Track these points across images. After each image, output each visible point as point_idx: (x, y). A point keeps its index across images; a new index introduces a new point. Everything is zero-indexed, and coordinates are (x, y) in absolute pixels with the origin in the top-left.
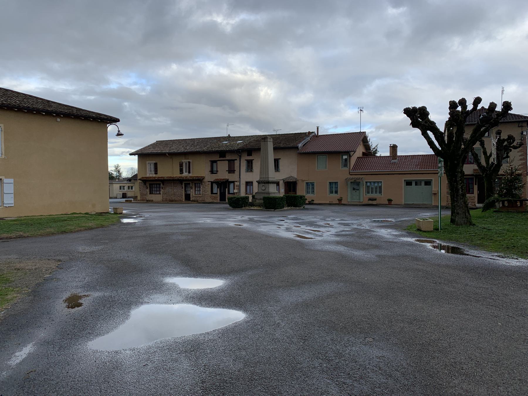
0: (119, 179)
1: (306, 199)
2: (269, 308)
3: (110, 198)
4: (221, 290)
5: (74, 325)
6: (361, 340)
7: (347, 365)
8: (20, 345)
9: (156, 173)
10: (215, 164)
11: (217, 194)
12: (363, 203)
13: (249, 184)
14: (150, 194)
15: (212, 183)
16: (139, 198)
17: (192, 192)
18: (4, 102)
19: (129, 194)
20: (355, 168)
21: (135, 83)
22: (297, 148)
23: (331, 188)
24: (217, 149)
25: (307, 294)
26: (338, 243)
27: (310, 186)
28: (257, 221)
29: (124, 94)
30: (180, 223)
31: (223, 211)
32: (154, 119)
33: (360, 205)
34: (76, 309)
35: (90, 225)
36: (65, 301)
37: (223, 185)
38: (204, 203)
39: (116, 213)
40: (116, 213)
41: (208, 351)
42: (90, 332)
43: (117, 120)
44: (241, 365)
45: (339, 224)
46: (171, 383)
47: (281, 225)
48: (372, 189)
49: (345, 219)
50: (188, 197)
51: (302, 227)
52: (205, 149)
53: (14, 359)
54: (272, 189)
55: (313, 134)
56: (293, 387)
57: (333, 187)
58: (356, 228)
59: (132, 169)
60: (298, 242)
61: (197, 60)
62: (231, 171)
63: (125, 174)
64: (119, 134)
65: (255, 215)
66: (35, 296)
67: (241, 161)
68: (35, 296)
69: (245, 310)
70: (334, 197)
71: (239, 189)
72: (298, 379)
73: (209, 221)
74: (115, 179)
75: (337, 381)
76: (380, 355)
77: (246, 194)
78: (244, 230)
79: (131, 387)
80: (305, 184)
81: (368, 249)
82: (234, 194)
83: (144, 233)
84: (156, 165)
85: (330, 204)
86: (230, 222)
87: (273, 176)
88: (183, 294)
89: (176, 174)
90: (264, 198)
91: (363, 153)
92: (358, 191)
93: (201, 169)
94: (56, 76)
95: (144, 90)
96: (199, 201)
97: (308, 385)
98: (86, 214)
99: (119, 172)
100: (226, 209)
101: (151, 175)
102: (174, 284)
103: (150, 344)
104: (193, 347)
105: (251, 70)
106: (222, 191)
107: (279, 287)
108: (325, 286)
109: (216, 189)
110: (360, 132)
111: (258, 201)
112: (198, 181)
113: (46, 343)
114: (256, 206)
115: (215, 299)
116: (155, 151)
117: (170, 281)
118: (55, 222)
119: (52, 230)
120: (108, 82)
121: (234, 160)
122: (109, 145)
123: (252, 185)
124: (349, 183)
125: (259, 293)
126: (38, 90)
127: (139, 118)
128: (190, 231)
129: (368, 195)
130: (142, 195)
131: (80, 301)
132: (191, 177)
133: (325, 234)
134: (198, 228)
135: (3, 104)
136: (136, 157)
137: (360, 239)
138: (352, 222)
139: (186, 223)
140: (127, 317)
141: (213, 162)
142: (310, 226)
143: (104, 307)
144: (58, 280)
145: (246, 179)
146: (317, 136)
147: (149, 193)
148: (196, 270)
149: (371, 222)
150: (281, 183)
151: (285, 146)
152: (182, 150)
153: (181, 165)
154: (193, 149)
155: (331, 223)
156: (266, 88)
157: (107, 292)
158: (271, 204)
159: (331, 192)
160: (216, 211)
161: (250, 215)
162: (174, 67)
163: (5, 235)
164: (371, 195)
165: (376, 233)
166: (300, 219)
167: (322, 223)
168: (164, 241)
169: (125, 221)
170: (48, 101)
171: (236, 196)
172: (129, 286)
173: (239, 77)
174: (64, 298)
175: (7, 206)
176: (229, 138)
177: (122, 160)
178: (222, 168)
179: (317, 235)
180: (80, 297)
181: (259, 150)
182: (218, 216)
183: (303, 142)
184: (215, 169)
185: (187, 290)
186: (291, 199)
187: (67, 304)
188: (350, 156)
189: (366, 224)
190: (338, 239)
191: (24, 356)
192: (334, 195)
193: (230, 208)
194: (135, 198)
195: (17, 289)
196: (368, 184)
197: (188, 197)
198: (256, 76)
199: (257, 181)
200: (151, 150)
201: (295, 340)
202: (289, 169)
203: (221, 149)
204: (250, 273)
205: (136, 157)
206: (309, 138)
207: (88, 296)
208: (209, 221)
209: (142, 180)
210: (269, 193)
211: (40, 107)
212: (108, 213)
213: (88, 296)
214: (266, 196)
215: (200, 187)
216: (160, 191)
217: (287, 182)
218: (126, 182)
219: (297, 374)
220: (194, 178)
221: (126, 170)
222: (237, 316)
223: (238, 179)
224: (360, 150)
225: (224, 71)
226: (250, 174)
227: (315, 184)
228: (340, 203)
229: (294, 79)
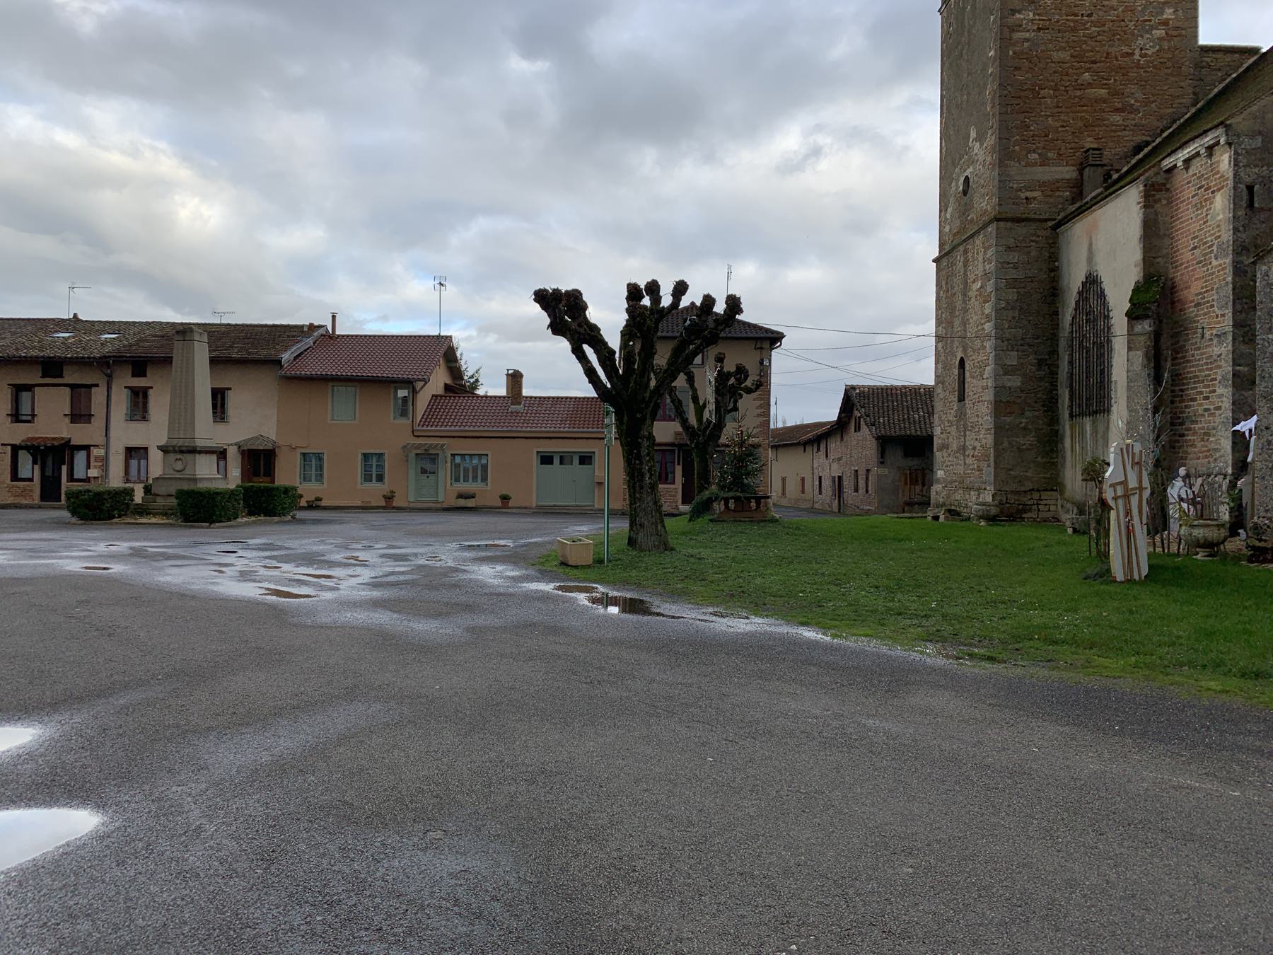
1: (301, 496)
4: (26, 756)
11: (31, 480)
15: (15, 449)
20: (427, 419)
22: (279, 362)
24: (34, 353)
25: (285, 740)
26: (376, 604)
27: (313, 462)
33: (437, 510)
45: (383, 556)
48: (466, 470)
49: (397, 544)
54: (205, 471)
55: (322, 331)
57: (373, 465)
60: (271, 606)
62: (79, 415)
65: (151, 540)
70: (375, 491)
71: (105, 466)
77: (127, 481)
78: (113, 581)
81: (448, 614)
82: (88, 480)
85: (365, 508)
87: (206, 431)
90: (181, 495)
92: (432, 477)
100: (60, 525)
105: (153, 148)
106: (49, 473)
107: (209, 729)
109: (27, 466)
110: (439, 337)
111: (160, 502)
114: (155, 515)
121: (90, 387)
133: (344, 585)
137: (432, 592)
138: (415, 551)
141: (18, 389)
142: (307, 565)
145: (119, 439)
150: (232, 453)
151: (244, 355)
155: (362, 555)
156: (196, 200)
158: (199, 509)
159: (368, 478)
160: (27, 530)
161: (137, 540)
166: (281, 548)
167: (337, 557)
171: (92, 486)
173: (116, 160)
176: (74, 323)
181: (167, 361)
182: (31, 545)
184: (25, 409)
186: (260, 495)
189: (447, 555)
190: (376, 594)
192: (374, 485)
193: (74, 520)
196: (458, 459)
198: (167, 164)
201: (241, 866)
202: (255, 416)
203: (48, 353)
204: (121, 702)
206: (310, 341)
210: (195, 480)
222: (78, 822)
224: (439, 379)
225: (66, 138)
226: (140, 426)
228: (389, 504)
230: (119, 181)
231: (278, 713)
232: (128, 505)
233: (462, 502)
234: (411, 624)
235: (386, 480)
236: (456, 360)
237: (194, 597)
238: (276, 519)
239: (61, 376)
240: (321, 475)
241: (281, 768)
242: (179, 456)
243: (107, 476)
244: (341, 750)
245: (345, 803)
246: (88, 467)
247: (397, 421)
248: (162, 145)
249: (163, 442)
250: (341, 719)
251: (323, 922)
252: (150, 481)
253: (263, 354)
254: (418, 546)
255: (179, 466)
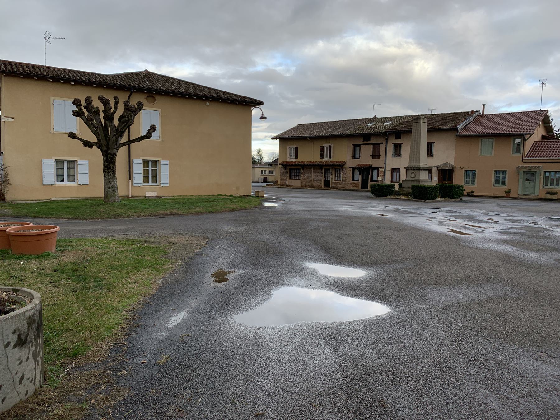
0: (260, 163)
1: (465, 190)
2: (417, 305)
3: (253, 182)
4: (363, 280)
5: (221, 298)
6: (531, 354)
7: (512, 378)
8: (176, 310)
9: (296, 157)
10: (357, 149)
11: (358, 181)
12: (539, 197)
13: (396, 170)
14: (290, 179)
15: (354, 169)
16: (279, 183)
17: (332, 178)
18: (162, 88)
19: (270, 179)
20: (529, 154)
21: (280, 64)
22: (456, 130)
23: (497, 178)
24: (361, 132)
25: (463, 295)
26: (504, 242)
27: (470, 175)
28: (404, 211)
29: (270, 76)
30: (319, 209)
31: (365, 199)
32: (298, 101)
33: (534, 200)
34: (222, 284)
35: (234, 206)
36: (213, 275)
37: (366, 171)
38: (344, 190)
39: (257, 197)
40: (257, 197)
41: (350, 341)
42: (235, 306)
43: (261, 103)
44: (385, 360)
45: (506, 220)
46: (311, 366)
47: (432, 218)
48: (552, 180)
49: (513, 215)
50: (327, 184)
51: (459, 221)
52: (348, 132)
53: (170, 322)
54: (423, 177)
55: (477, 114)
56: (445, 392)
57: (500, 177)
58: (528, 226)
59: (273, 153)
60: (453, 237)
61: (345, 35)
62: (376, 155)
63: (267, 159)
64: (263, 118)
65: (402, 205)
66: (187, 268)
67: (388, 145)
68: (187, 268)
69: (390, 304)
70: (501, 189)
71: (384, 176)
72: (450, 384)
73: (349, 209)
74: (257, 163)
75: (498, 394)
76: (556, 374)
77: (392, 182)
78: (389, 220)
79: (273, 364)
80: (464, 172)
81: (543, 251)
82: (377, 181)
83: (284, 217)
84: (296, 149)
85: (495, 197)
86: (372, 212)
87: (425, 161)
88: (323, 281)
89: (316, 159)
90: (413, 187)
91: (542, 136)
92: (532, 183)
93: (342, 154)
94: (207, 61)
95: (288, 71)
96: (339, 188)
97: (462, 392)
98: (231, 196)
99: (261, 156)
100: (368, 198)
101: (291, 160)
102: (314, 269)
103: (291, 325)
104: (334, 334)
105: (407, 43)
106: (364, 178)
107: (430, 284)
108: (485, 288)
109: (357, 176)
110: (540, 111)
111: (405, 190)
112: (339, 167)
113: (197, 312)
114: (403, 195)
115: (357, 289)
116: (291, 135)
117: (310, 266)
118: (204, 202)
119: (201, 209)
120: (254, 64)
121: (379, 144)
122: (253, 129)
123: (399, 172)
124: (521, 172)
125: (406, 289)
126: (191, 76)
127: (282, 101)
128: (329, 218)
129: (547, 187)
130: (282, 179)
131: (226, 277)
132: (331, 162)
133: (487, 231)
134: (338, 216)
135: (161, 89)
136: (278, 140)
137: (533, 239)
138: (523, 219)
139: (325, 209)
140: (269, 296)
141: (355, 146)
142: (469, 221)
143: (247, 284)
144: (206, 255)
145: (392, 164)
146: (482, 116)
147: (288, 178)
148: (336, 257)
149: (549, 220)
150: (434, 170)
151: (441, 127)
152: (324, 133)
153: (322, 150)
154: (335, 132)
155: (495, 219)
156: (423, 61)
157: (250, 271)
158: (421, 194)
159: (497, 183)
160: (357, 199)
161: (396, 205)
162: (321, 44)
163: (161, 212)
164: (550, 188)
165: (555, 234)
166: (456, 212)
167: (484, 218)
168: (304, 227)
169: (266, 204)
170: (199, 86)
171: (379, 183)
172: (270, 267)
173: (392, 50)
174: (212, 273)
175: (163, 185)
176: (375, 119)
177: (265, 145)
178: (366, 152)
179: (476, 232)
180: (226, 273)
181: (410, 132)
182: (359, 204)
183: (465, 123)
184: (357, 154)
185: (327, 277)
186: (446, 189)
187: (214, 278)
188: (525, 140)
189: (542, 222)
190: (504, 237)
191: (179, 321)
192: (500, 186)
193: (373, 196)
194: (276, 182)
195: (173, 261)
196: (547, 174)
197: (327, 184)
198: (413, 49)
199: (405, 168)
200: (293, 133)
201: (447, 342)
202: (445, 154)
203: (366, 132)
204: (395, 267)
205: (278, 141)
206: (471, 119)
207: (232, 273)
208: (349, 209)
209: (283, 165)
210: (419, 182)
211: (192, 91)
212: (250, 196)
213: (232, 273)
214: (415, 185)
215: (340, 173)
216: (299, 176)
217: (453, 171)
218: (267, 166)
219: (448, 378)
220: (335, 163)
221: (267, 155)
222: (378, 309)
223: (383, 165)
224: (539, 133)
225: (374, 45)
226: (397, 159)
227: (477, 172)
228: (508, 196)
229: (457, 48)
230: (391, 59)
231: (459, 283)
232: (393, 191)
233: (549, 196)
234: (523, 253)
235: (507, 184)
236: (549, 122)
237: (420, 230)
238: (453, 200)
239: (370, 141)
240: (474, 181)
241: (460, 307)
242: (413, 171)
243: (384, 180)
244: (490, 304)
245: (493, 328)
246: (378, 176)
247: (513, 155)
248: (410, 40)
249: (407, 165)
250: (489, 291)
251: (485, 377)
252: (401, 182)
253: (449, 126)
254: (524, 216)
255: (413, 175)
